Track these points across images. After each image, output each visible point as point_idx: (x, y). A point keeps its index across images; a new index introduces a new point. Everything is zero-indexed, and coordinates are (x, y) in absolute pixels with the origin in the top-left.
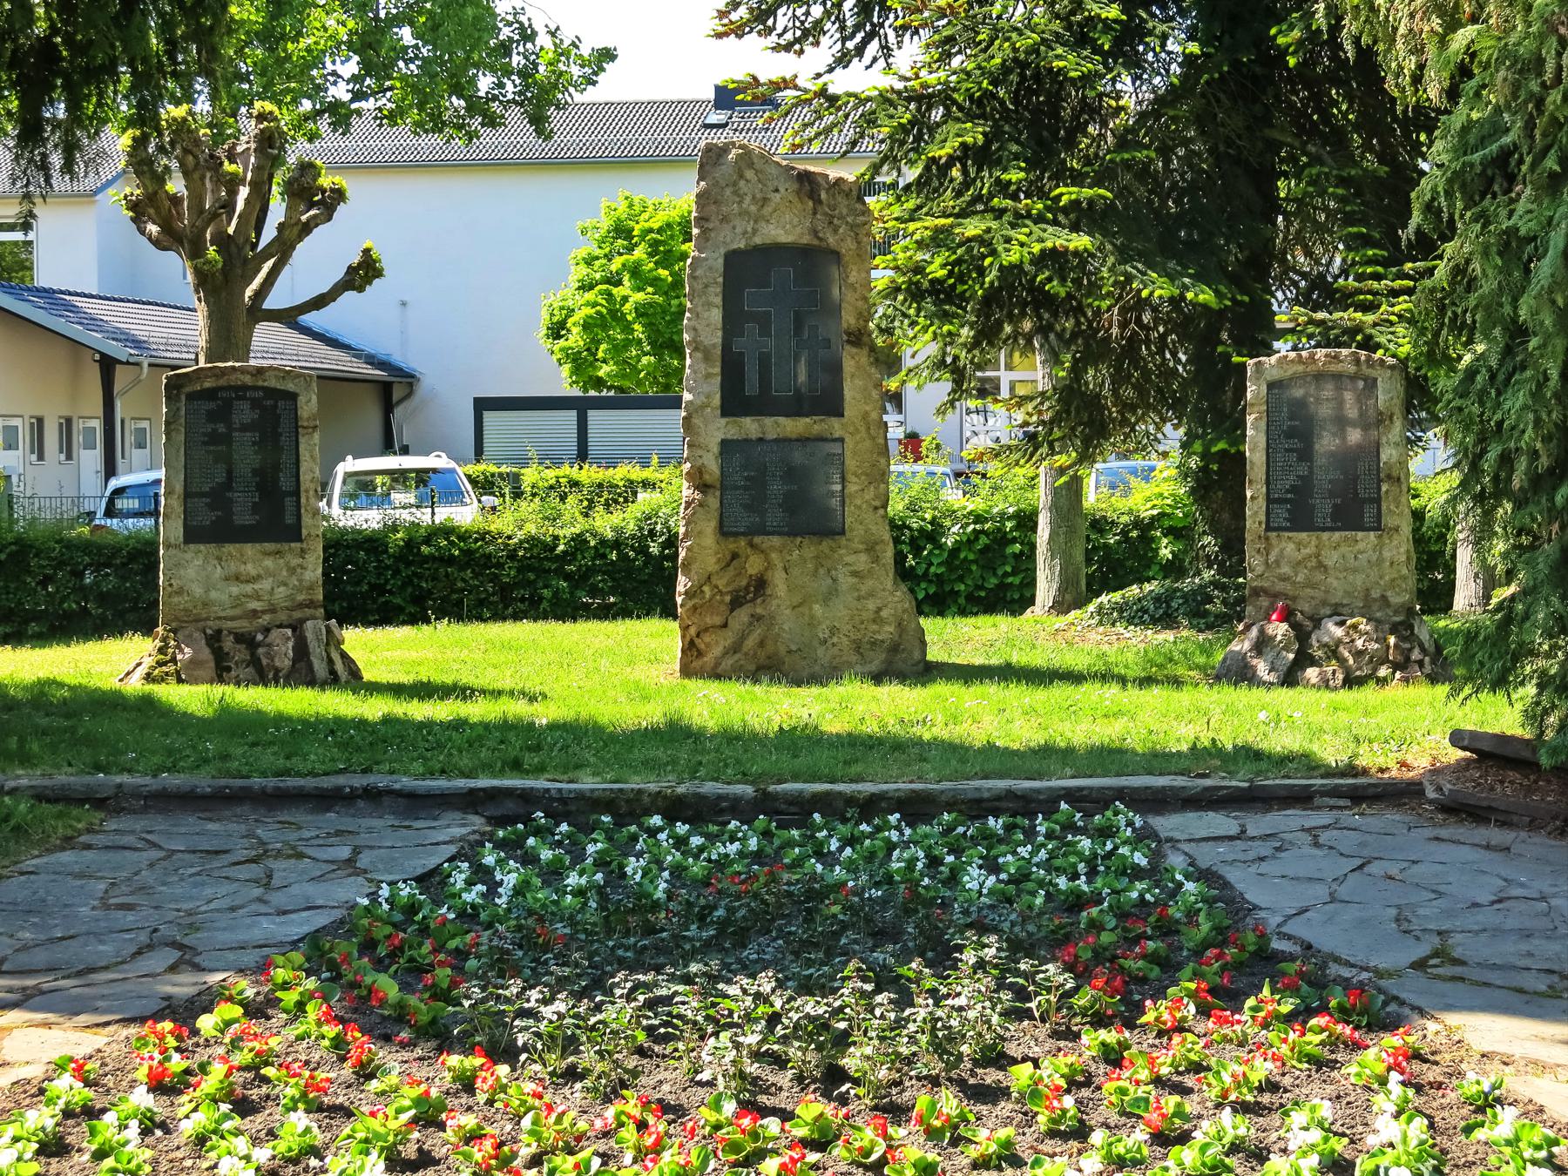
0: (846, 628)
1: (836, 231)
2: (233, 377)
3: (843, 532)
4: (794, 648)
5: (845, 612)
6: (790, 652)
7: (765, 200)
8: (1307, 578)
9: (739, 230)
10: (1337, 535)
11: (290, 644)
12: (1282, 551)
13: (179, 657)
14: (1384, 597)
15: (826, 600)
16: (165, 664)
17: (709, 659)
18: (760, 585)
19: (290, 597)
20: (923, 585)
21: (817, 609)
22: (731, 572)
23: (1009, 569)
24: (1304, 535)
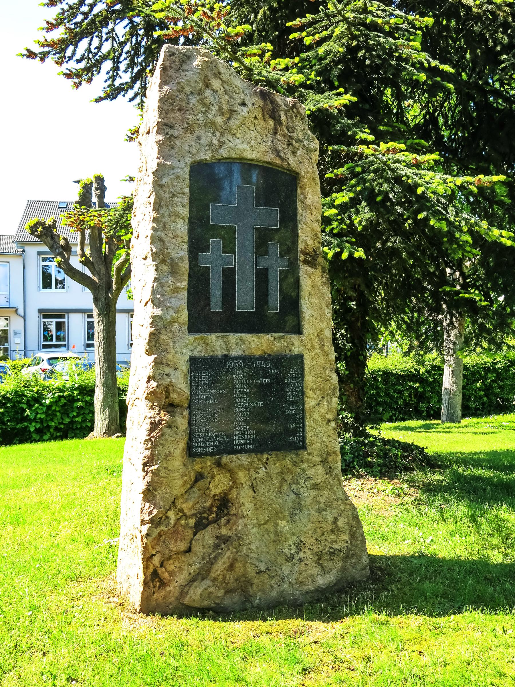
0: (309, 541)
1: (294, 153)
3: (304, 447)
4: (262, 568)
5: (309, 526)
6: (259, 573)
9: (204, 141)
17: (173, 588)
21: (283, 525)
22: (196, 493)
23: (75, 414)
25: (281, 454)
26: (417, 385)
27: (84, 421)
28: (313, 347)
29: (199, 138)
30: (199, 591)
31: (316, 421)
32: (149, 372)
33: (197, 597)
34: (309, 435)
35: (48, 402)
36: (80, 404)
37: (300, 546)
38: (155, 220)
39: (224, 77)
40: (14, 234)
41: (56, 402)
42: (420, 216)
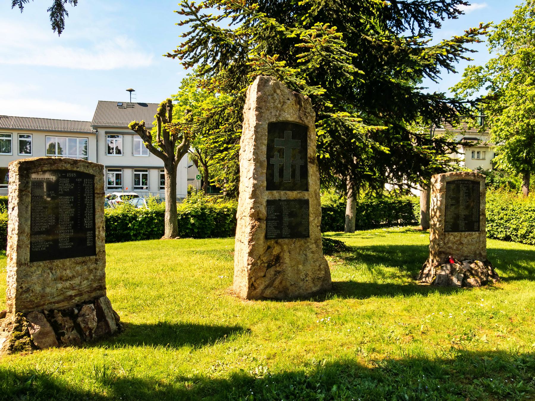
0: (310, 273)
1: (307, 118)
2: (60, 165)
3: (308, 236)
5: (310, 267)
6: (291, 285)
7: (284, 102)
8: (457, 247)
10: (467, 233)
11: (95, 313)
12: (449, 238)
13: (31, 332)
14: (480, 253)
15: (304, 264)
16: (22, 337)
17: (259, 290)
18: (278, 259)
19: (90, 286)
20: (132, 231)
24: (456, 233)
25: (300, 239)
26: (332, 213)
27: (159, 230)
28: (312, 196)
29: (271, 113)
30: (269, 291)
31: (313, 226)
32: (251, 205)
33: (268, 294)
34: (311, 232)
35: (140, 220)
36: (156, 221)
37: (306, 275)
38: (255, 145)
39: (281, 88)
40: (91, 121)
41: (144, 220)
42: (352, 141)
